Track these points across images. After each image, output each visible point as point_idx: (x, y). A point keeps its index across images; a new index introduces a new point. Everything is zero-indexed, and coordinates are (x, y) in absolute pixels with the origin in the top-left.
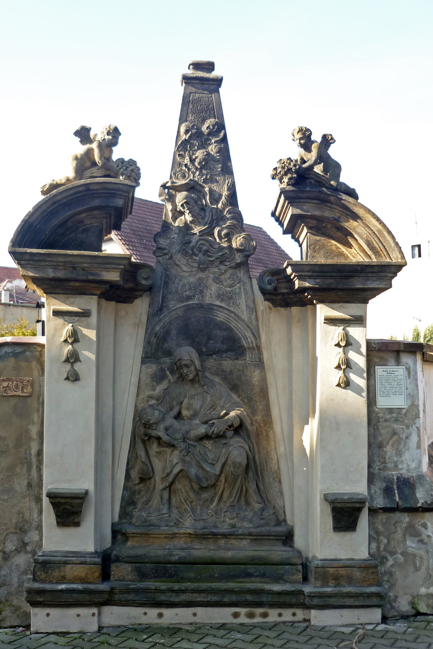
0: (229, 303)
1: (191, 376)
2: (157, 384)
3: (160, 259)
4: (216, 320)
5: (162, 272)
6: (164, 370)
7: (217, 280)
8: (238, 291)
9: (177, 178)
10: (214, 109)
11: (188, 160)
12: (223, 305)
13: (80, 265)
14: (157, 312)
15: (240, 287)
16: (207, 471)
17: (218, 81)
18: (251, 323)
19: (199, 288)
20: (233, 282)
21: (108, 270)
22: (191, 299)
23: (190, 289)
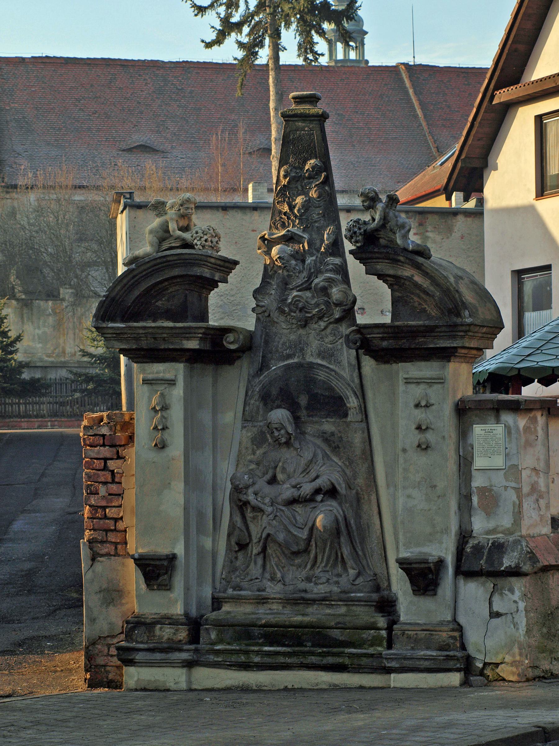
0: (330, 361)
1: (283, 440)
2: (257, 448)
3: (260, 316)
4: (317, 379)
5: (262, 330)
6: (264, 432)
8: (339, 347)
9: (277, 228)
10: (315, 148)
11: (287, 208)
12: (324, 363)
13: (160, 336)
14: (257, 372)
15: (342, 343)
16: (295, 536)
18: (353, 381)
19: (299, 347)
20: (334, 338)
21: (188, 339)
22: (292, 358)
23: (290, 347)
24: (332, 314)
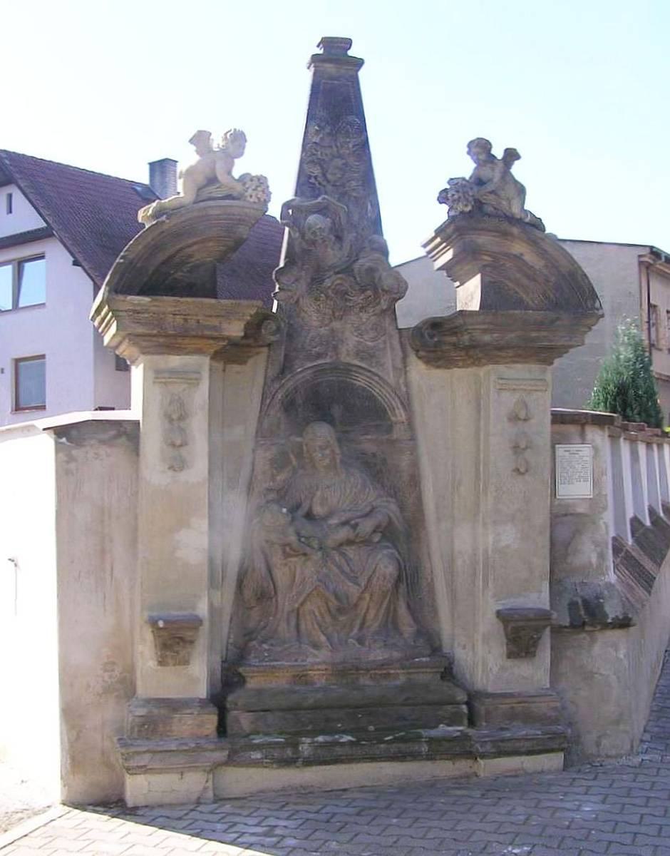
7: (359, 331)
12: (363, 365)
17: (359, 63)
19: (333, 342)
23: (321, 344)
24: (379, 303)
